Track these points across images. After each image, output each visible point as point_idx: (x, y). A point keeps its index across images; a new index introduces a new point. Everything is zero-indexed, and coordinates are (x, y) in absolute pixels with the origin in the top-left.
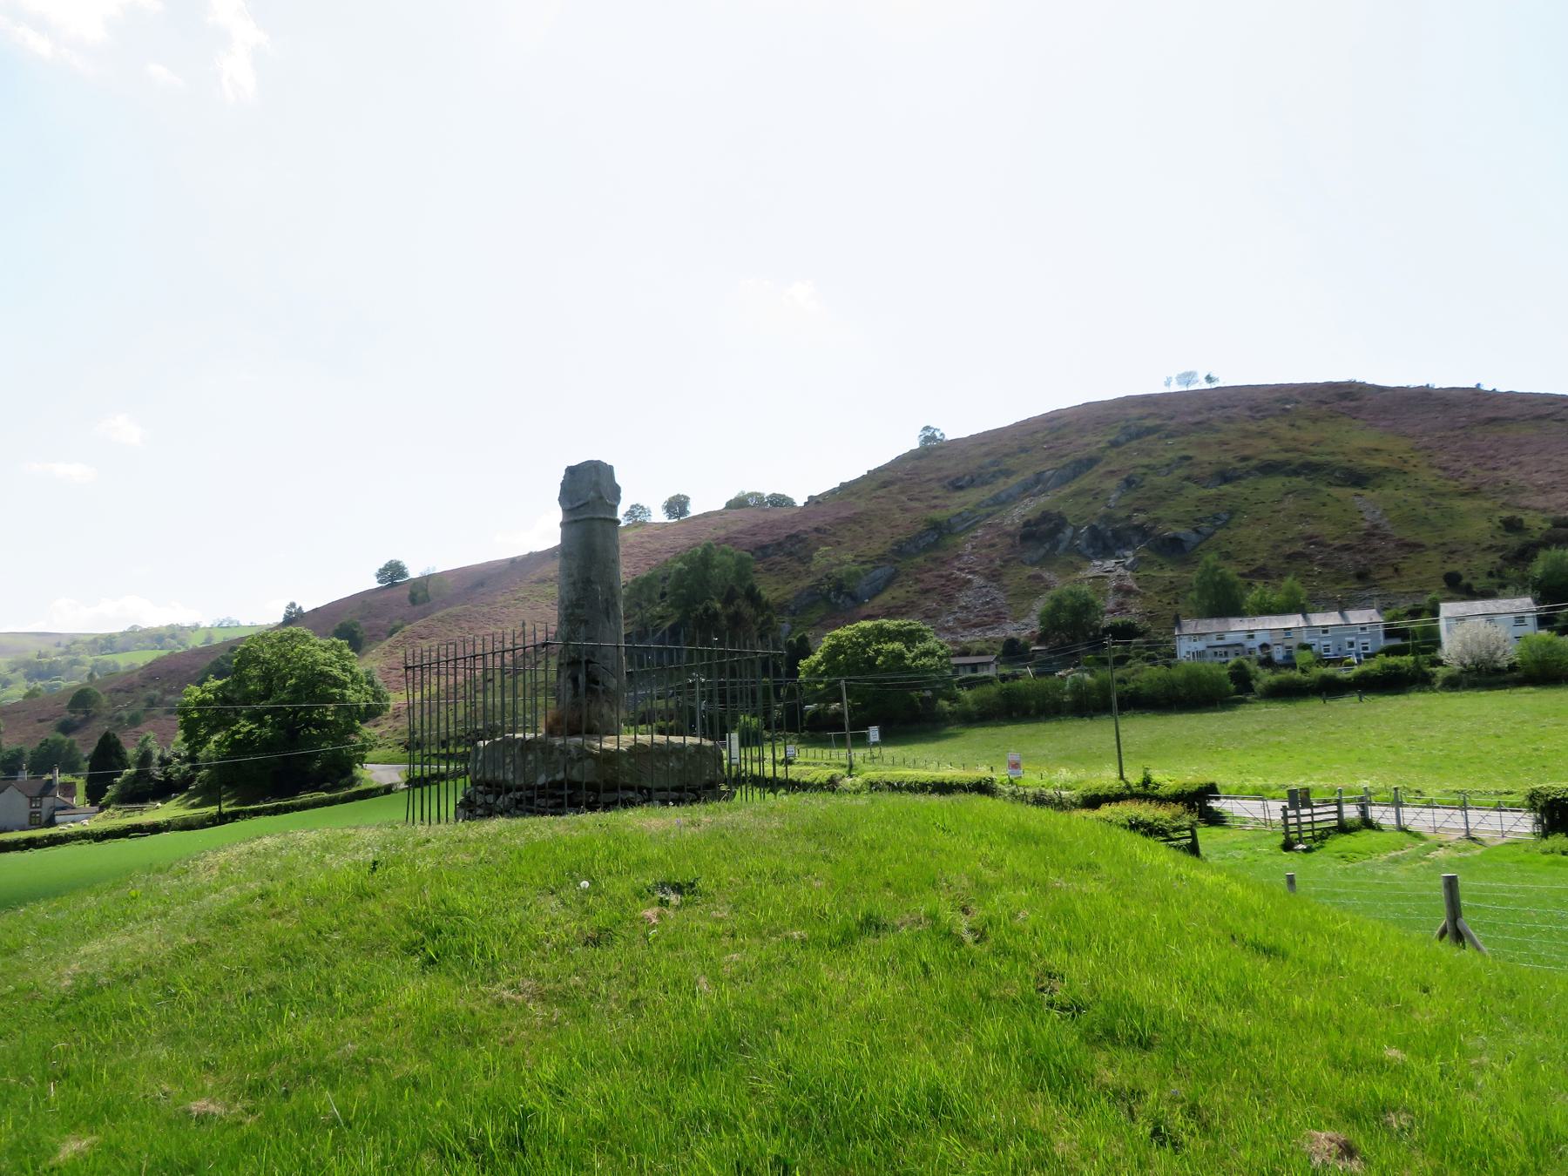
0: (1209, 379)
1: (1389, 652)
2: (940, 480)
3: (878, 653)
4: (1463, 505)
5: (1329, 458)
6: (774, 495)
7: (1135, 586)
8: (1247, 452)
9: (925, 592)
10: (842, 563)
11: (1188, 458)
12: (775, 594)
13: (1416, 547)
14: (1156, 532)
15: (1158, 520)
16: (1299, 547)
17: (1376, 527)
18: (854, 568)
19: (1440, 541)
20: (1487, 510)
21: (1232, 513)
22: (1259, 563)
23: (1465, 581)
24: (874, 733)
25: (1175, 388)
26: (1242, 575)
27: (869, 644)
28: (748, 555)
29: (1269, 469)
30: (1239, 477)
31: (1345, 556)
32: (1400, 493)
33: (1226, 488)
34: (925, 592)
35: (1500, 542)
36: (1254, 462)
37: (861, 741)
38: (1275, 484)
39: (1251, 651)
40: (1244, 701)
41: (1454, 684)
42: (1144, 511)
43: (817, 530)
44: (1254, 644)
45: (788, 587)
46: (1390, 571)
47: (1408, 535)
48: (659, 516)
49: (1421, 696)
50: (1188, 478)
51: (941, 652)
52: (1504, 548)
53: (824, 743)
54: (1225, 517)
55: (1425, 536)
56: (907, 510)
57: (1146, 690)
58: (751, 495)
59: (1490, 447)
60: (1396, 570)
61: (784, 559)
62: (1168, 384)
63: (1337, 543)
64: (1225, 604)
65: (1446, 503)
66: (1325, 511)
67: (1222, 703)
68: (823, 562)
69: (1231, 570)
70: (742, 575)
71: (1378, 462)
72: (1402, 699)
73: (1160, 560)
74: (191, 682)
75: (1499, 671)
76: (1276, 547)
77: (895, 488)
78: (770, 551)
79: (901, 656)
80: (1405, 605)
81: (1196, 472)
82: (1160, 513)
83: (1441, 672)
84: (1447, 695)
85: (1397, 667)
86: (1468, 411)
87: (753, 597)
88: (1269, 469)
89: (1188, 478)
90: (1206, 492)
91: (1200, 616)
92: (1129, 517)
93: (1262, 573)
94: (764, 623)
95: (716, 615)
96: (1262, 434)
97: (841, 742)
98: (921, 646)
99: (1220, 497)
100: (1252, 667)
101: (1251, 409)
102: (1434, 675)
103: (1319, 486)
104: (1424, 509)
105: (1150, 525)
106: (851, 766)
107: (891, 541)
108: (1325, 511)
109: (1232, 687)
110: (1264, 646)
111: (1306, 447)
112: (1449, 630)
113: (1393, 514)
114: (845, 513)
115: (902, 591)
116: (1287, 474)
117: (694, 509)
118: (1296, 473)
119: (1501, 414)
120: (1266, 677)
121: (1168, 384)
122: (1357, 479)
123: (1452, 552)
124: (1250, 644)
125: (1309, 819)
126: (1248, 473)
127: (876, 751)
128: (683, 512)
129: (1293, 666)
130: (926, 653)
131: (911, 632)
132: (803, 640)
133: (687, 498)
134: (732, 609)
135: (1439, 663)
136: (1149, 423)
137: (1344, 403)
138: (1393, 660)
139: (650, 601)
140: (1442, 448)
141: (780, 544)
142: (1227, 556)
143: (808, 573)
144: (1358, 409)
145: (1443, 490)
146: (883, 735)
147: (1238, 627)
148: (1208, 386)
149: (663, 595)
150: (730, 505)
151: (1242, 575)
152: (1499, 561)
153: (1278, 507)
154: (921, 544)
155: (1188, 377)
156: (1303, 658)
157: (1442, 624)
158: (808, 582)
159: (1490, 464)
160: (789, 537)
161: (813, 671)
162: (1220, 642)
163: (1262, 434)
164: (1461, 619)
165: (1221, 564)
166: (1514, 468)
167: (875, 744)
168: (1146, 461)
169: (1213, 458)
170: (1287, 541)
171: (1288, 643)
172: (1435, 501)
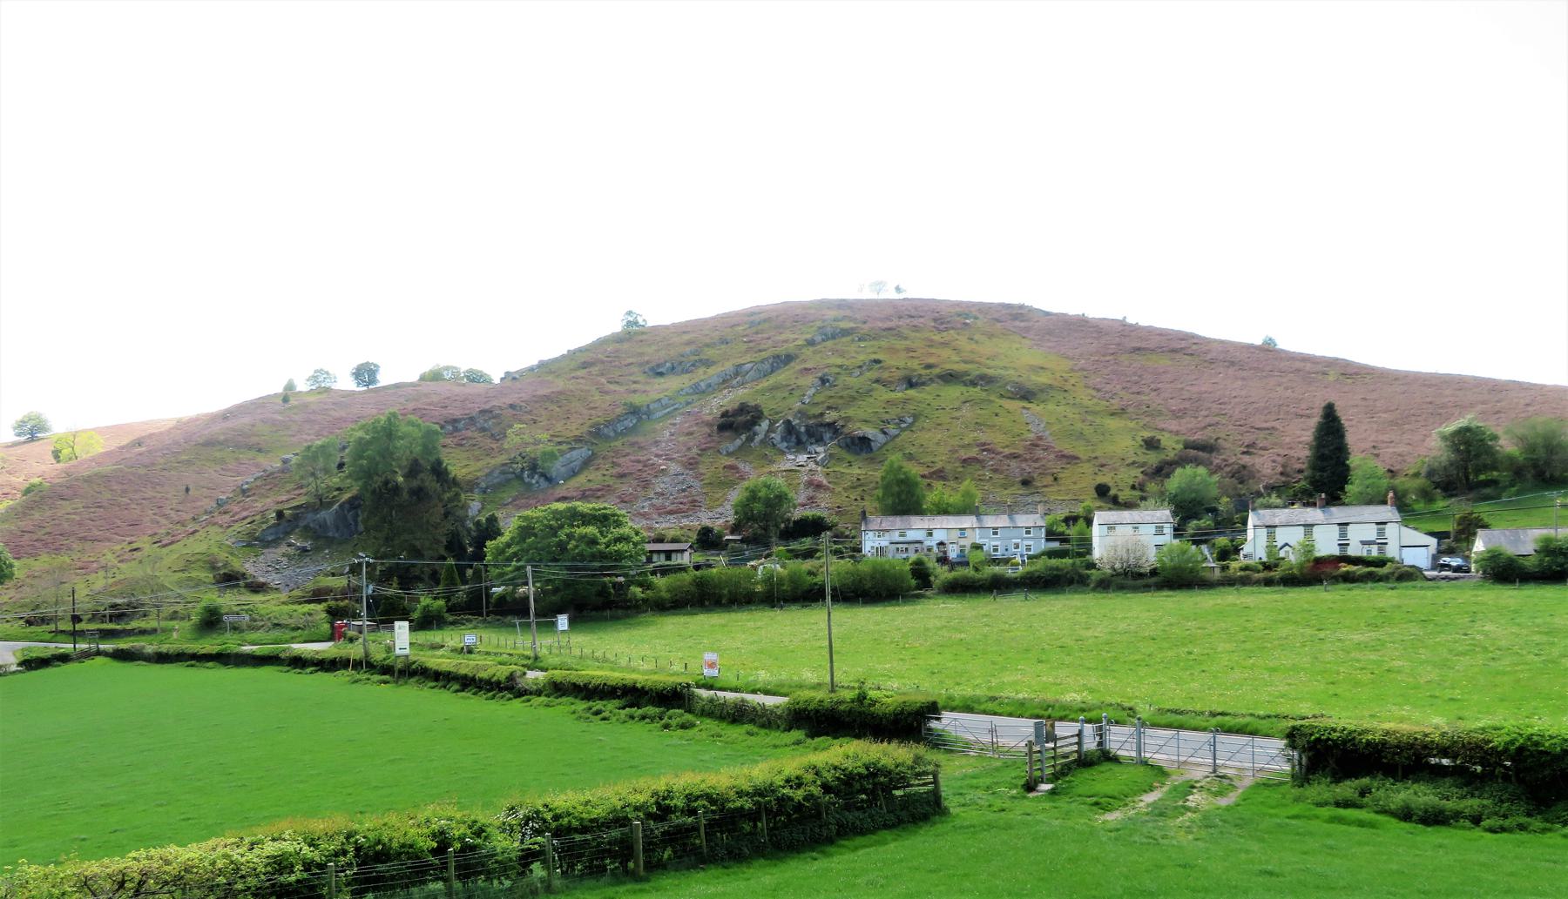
0: (898, 289)
2: (641, 365)
3: (570, 536)
4: (1113, 424)
5: (1002, 372)
8: (931, 360)
9: (622, 476)
11: (877, 361)
14: (846, 430)
15: (848, 419)
16: (974, 452)
17: (1040, 438)
20: (1132, 430)
22: (938, 466)
23: (1112, 492)
24: (563, 621)
30: (923, 384)
31: (1013, 463)
33: (911, 392)
35: (1141, 459)
36: (936, 371)
43: (512, 406)
45: (480, 464)
46: (1050, 479)
47: (1067, 447)
50: (877, 381)
51: (636, 539)
52: (1143, 465)
55: (1080, 450)
56: (607, 393)
58: (447, 368)
59: (1135, 374)
62: (861, 290)
63: (1007, 451)
65: (1098, 421)
66: (998, 421)
68: (517, 439)
69: (914, 470)
71: (1043, 379)
76: (954, 451)
77: (595, 370)
78: (461, 425)
80: (1062, 513)
81: (885, 375)
82: (851, 412)
85: (1057, 569)
87: (439, 472)
89: (877, 381)
92: (822, 414)
93: (940, 475)
96: (945, 344)
99: (906, 401)
101: (935, 320)
108: (998, 421)
109: (913, 582)
113: (1056, 428)
117: (384, 379)
118: (973, 384)
119: (1143, 345)
120: (942, 574)
127: (564, 640)
128: (372, 380)
135: (1092, 566)
137: (1017, 323)
138: (1054, 562)
140: (1096, 371)
142: (910, 457)
143: (501, 451)
144: (1027, 329)
146: (572, 622)
149: (341, 466)
150: (422, 378)
152: (1141, 477)
155: (879, 285)
157: (1096, 531)
159: (1135, 389)
160: (483, 412)
163: (945, 344)
165: (905, 464)
168: (839, 361)
169: (901, 364)
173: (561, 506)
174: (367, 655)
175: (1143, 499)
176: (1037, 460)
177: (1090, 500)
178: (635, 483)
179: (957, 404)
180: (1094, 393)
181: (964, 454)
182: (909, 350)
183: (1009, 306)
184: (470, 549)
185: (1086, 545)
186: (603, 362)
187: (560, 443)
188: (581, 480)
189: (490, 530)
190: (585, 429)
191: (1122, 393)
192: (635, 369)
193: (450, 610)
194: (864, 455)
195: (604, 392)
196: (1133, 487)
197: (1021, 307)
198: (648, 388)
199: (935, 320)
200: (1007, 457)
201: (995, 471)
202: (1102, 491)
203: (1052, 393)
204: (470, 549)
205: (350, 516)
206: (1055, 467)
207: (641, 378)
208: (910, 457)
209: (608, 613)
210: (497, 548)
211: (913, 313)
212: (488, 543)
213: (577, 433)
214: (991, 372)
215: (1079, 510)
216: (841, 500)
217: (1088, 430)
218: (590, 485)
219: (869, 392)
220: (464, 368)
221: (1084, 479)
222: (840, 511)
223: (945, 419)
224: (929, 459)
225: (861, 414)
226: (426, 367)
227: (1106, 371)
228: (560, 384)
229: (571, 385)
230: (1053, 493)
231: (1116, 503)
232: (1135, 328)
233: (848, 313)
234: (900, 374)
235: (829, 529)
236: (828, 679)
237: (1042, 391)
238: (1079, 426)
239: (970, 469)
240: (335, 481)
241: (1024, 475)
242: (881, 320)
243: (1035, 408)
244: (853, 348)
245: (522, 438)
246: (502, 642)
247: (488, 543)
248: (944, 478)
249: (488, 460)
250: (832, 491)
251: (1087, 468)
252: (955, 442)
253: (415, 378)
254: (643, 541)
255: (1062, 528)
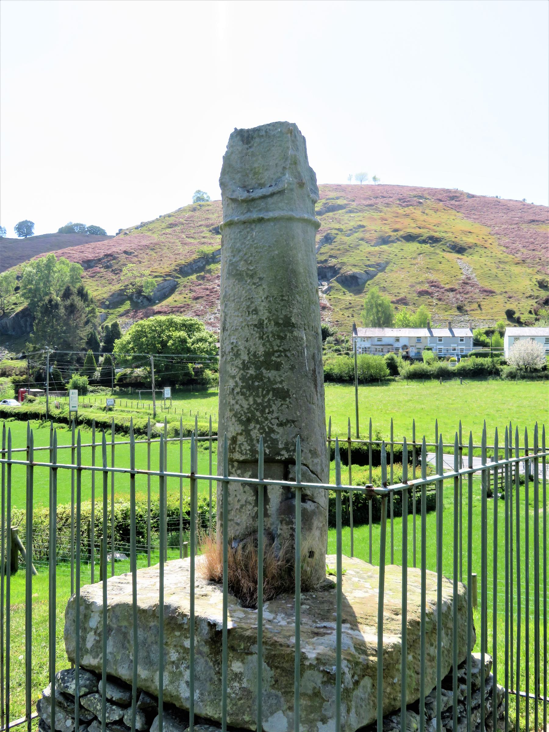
0: (375, 179)
1: (477, 355)
2: (207, 226)
3: (170, 337)
4: (516, 270)
5: (444, 235)
6: (92, 227)
7: (328, 305)
8: (397, 226)
9: (196, 298)
10: (142, 275)
11: (363, 226)
12: (95, 293)
13: (491, 293)
14: (342, 271)
15: (343, 264)
16: (426, 287)
17: (469, 279)
18: (150, 279)
19: (504, 290)
20: (529, 274)
21: (387, 263)
22: (402, 296)
23: (516, 316)
24: (167, 391)
25: (354, 182)
26: (392, 302)
27: (163, 331)
28: (79, 266)
29: (410, 238)
30: (393, 242)
31: (451, 294)
32: (483, 259)
33: (385, 247)
34: (196, 298)
35: (536, 293)
36: (401, 233)
37: (160, 395)
38: (414, 246)
39: (397, 349)
40: (394, 380)
41: (512, 376)
42: (335, 257)
43: (125, 252)
44: (399, 345)
45: (105, 289)
46: (475, 306)
47: (486, 285)
48: (12, 234)
49: (494, 382)
50: (362, 239)
51: (210, 340)
52: (537, 297)
53: (133, 396)
54: (384, 266)
55: (495, 286)
56: (185, 244)
57: (336, 371)
58: (77, 225)
59: (531, 237)
60: (479, 306)
61: (102, 270)
62: (350, 179)
63: (447, 287)
64: (384, 320)
65: (507, 267)
66: (440, 266)
67: (381, 381)
68: (130, 274)
69: (387, 298)
70: (75, 279)
71: (470, 240)
72: (484, 383)
73: (344, 290)
74: (75, 232)
75: (536, 370)
76: (412, 286)
77: (178, 229)
78: (92, 264)
79: (184, 341)
80: (483, 328)
81: (367, 235)
82: (345, 259)
83: (506, 369)
84: (510, 382)
85: (482, 365)
86: (519, 214)
87: (82, 294)
88: (410, 238)
89: (362, 239)
90: (372, 249)
91: (367, 326)
92: (326, 261)
93: (403, 301)
94: (90, 312)
95: (57, 306)
96: (407, 215)
97: (147, 396)
98: (197, 335)
99: (380, 253)
100: (399, 360)
101: (400, 200)
102: (502, 370)
103: (438, 251)
104: (496, 270)
105: (339, 266)
106: (155, 415)
107: (175, 263)
108: (440, 266)
109: (388, 371)
110: (405, 347)
111: (431, 226)
112: (510, 344)
113: (479, 272)
114: (145, 242)
115: (181, 297)
116: (420, 242)
117: (37, 232)
118: (424, 242)
119: (537, 218)
120: (405, 367)
121: (350, 179)
122: (460, 250)
123: (510, 298)
124: (396, 345)
125: (449, 460)
126: (398, 239)
127: (168, 402)
128: (29, 232)
129: (421, 360)
130: (201, 340)
131: (191, 325)
132: (115, 326)
133: (32, 224)
134: (68, 302)
135: (504, 363)
136: (340, 202)
137: (453, 202)
138: (480, 360)
139: (7, 291)
140: (505, 235)
141: (100, 260)
142: (384, 289)
143: (119, 281)
144: (460, 207)
145: (506, 260)
146: (174, 391)
147: (389, 333)
148: (373, 183)
149: (17, 289)
150: (61, 231)
151: (392, 302)
152: (535, 305)
153: (414, 262)
154: (195, 267)
155: (362, 177)
156: (427, 355)
157: (506, 341)
158: (117, 287)
159: (531, 247)
160: (107, 256)
161: (124, 348)
162: (379, 343)
163: (407, 215)
164: (517, 338)
165: (381, 294)
166: (543, 250)
167: (167, 398)
168: (337, 226)
169: (378, 229)
170: (419, 283)
171: (419, 346)
172: (501, 266)
173: (162, 318)
174: (48, 411)
175: (537, 320)
176: (467, 293)
177: (502, 319)
178: (205, 303)
179: (414, 255)
180: (505, 249)
181: (419, 288)
182: (383, 219)
183: (448, 191)
184: (102, 344)
185: (499, 347)
186: (183, 224)
187: (156, 277)
188: (170, 301)
189: (113, 333)
190: (173, 267)
191: (523, 250)
192: (205, 229)
193: (91, 383)
194: (353, 288)
195: (184, 244)
196: (530, 312)
197: (456, 191)
198: (212, 241)
199: (400, 200)
200: (447, 290)
201: (440, 300)
202: (510, 314)
203: (477, 249)
204: (102, 344)
205: (22, 322)
206: (479, 297)
207: (208, 234)
208: (384, 289)
209: (191, 387)
210: (122, 344)
211: (385, 194)
212: (116, 341)
213: (167, 270)
214: (436, 235)
215: (495, 326)
216: (339, 317)
217: (501, 274)
218: (175, 304)
219: (357, 247)
220: (88, 224)
221: (497, 307)
222: (338, 323)
223: (406, 264)
224: (397, 291)
225: (351, 260)
226: (63, 224)
227: (512, 235)
228: (156, 238)
229: (163, 239)
230: (477, 315)
231: (519, 322)
232: (531, 206)
233: (342, 194)
234: (376, 235)
235: (332, 335)
236: (347, 432)
237: (470, 247)
238: (494, 271)
239: (422, 298)
240: (13, 299)
241: (461, 299)
242: (365, 199)
243: (465, 258)
244: (347, 217)
245: (141, 273)
246: (129, 404)
247: (116, 341)
248: (406, 304)
249: (110, 286)
250: (333, 311)
251: (500, 299)
252: (413, 280)
253: (55, 231)
254: (214, 341)
255: (483, 338)
